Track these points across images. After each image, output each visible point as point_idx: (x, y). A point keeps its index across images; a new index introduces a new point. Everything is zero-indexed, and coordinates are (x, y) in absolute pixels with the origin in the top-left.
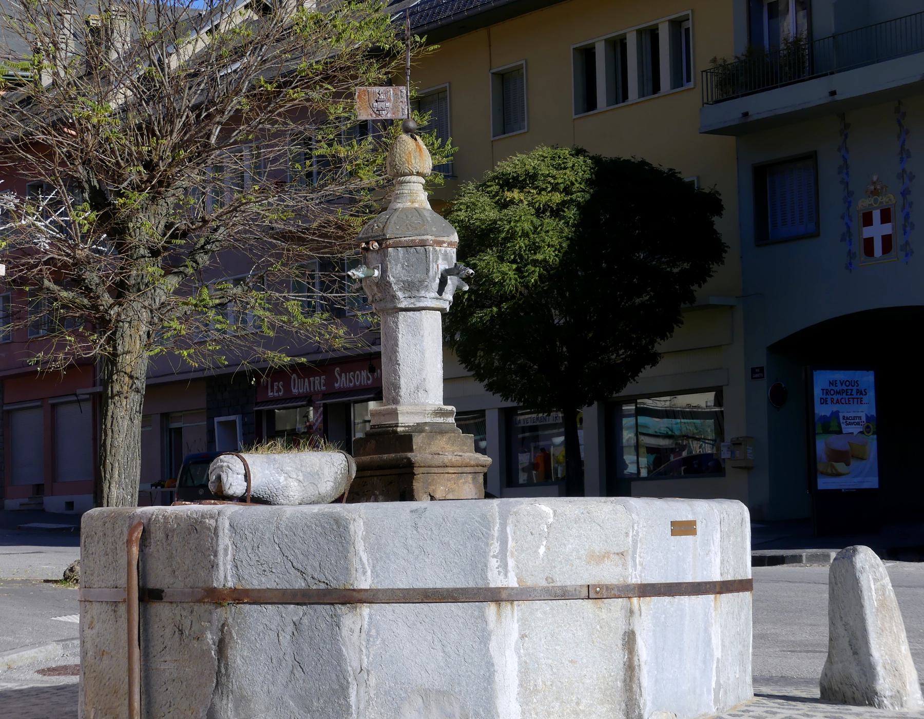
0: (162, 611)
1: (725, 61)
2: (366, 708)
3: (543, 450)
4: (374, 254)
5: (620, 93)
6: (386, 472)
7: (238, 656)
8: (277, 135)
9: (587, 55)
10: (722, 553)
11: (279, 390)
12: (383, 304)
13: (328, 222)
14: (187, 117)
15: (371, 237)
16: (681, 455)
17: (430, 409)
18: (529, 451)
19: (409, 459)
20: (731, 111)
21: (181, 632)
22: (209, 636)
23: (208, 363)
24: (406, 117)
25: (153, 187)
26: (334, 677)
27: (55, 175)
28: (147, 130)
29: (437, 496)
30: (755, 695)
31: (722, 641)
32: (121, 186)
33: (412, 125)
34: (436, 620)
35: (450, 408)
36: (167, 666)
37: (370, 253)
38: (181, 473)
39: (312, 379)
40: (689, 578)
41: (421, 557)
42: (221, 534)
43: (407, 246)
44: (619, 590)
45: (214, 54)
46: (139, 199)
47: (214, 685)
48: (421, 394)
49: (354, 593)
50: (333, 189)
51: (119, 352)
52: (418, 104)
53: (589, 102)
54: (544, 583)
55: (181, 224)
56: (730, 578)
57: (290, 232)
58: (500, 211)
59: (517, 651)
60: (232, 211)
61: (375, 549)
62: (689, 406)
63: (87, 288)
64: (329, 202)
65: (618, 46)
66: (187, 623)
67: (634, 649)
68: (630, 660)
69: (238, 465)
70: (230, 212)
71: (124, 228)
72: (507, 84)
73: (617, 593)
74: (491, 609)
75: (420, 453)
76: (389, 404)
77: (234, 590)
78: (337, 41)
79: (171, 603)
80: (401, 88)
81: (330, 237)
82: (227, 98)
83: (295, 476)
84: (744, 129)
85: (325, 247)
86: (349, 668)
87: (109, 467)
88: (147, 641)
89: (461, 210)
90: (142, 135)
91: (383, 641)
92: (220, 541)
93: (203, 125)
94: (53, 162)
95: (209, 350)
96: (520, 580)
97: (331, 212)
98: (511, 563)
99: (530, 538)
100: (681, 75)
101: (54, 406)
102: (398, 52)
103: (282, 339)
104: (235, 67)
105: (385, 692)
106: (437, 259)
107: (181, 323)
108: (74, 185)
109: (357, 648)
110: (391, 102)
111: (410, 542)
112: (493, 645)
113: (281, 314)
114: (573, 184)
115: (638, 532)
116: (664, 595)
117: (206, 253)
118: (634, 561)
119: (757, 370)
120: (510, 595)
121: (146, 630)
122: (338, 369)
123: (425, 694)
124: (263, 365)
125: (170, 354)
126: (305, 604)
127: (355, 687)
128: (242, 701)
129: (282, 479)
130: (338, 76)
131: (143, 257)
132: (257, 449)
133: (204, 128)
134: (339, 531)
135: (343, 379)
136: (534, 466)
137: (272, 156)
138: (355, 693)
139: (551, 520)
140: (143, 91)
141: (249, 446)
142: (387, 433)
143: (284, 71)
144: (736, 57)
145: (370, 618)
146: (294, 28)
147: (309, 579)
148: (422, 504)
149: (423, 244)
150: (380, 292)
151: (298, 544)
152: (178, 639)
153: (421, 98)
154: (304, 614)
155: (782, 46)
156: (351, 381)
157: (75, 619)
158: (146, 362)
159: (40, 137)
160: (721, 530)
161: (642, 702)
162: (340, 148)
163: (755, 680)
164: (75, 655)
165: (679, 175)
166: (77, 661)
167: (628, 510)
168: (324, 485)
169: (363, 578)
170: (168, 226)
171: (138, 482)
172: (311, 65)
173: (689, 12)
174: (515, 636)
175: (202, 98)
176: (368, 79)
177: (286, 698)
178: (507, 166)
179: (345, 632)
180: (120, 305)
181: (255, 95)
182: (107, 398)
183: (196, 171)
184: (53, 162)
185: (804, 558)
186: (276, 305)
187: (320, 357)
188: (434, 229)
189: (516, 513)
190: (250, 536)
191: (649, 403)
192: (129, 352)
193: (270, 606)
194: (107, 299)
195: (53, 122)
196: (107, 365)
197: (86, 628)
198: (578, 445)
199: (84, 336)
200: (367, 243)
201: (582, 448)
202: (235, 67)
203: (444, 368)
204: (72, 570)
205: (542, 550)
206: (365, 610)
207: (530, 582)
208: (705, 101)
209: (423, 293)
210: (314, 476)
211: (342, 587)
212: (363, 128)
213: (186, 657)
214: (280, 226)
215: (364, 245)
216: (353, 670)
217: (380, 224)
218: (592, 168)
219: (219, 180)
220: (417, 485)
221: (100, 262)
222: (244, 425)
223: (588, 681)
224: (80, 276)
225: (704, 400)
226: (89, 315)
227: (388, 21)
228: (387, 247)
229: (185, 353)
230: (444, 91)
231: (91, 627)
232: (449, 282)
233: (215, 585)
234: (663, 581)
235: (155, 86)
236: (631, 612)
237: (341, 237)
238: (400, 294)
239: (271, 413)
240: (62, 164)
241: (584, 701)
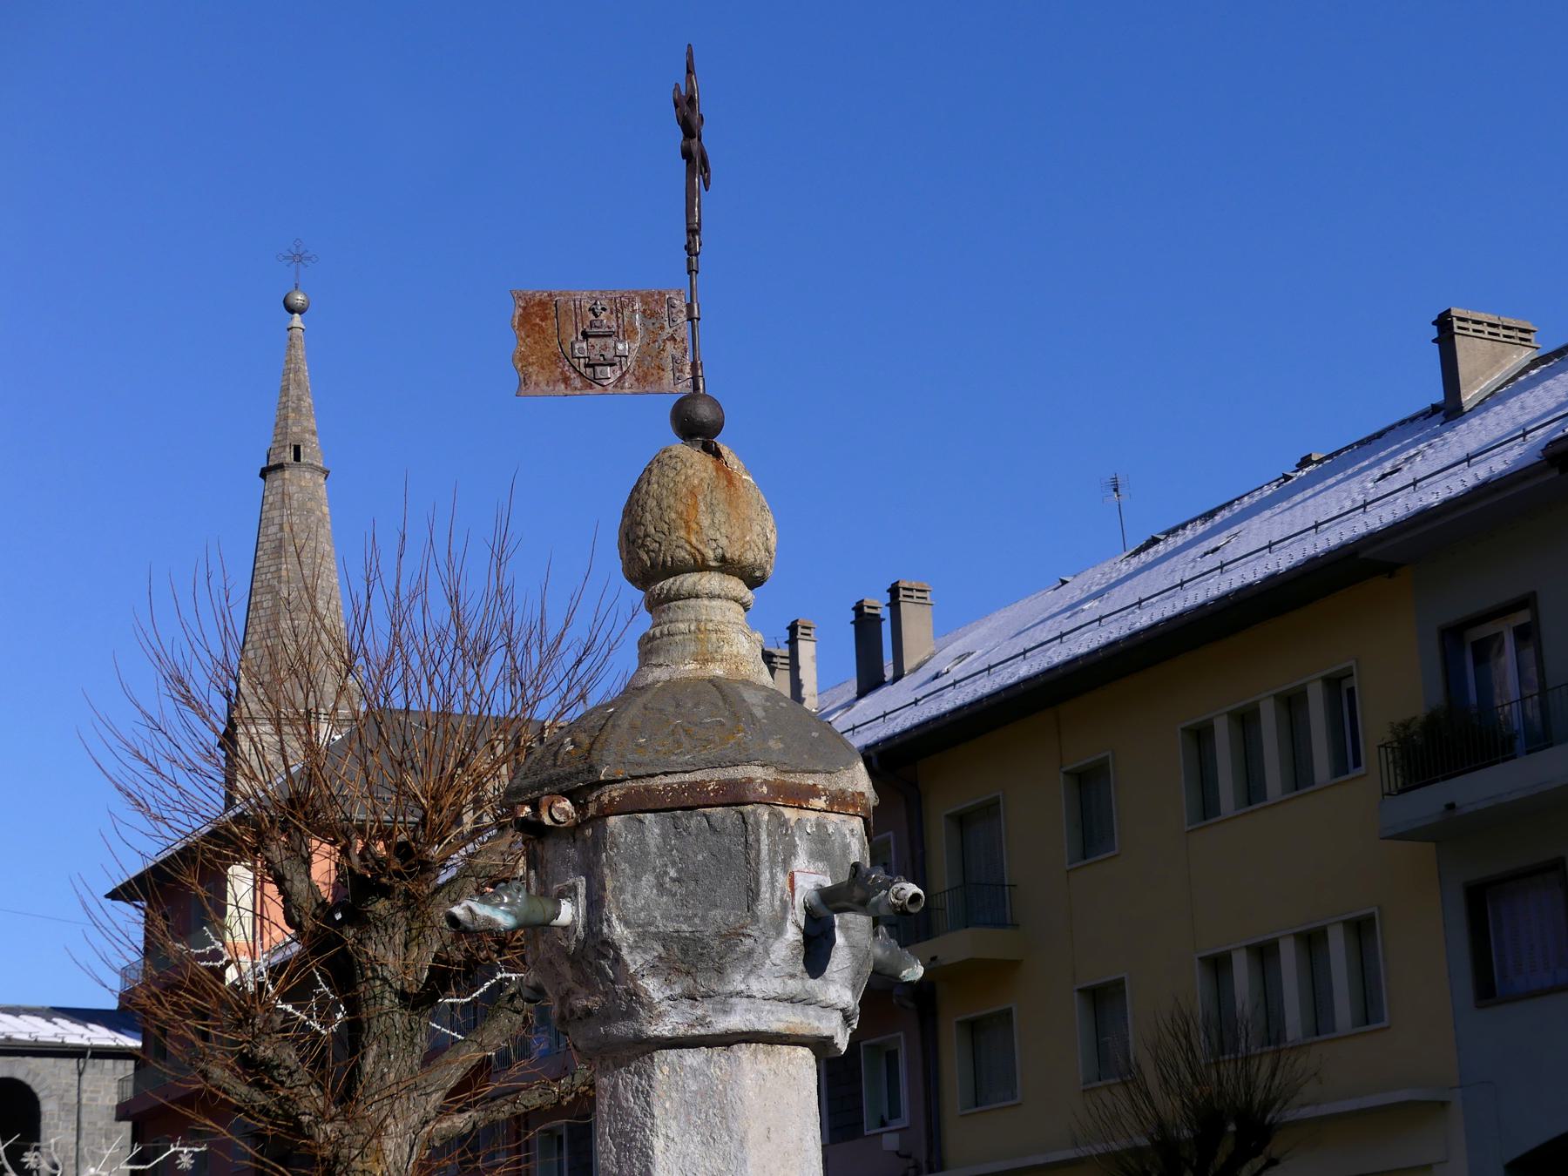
20: (1429, 801)
37: (550, 842)
53: (1208, 807)
72: (1088, 783)
84: (1450, 833)
106: (791, 852)
149: (734, 796)
188: (774, 744)
194: (311, 1100)
200: (535, 806)
209: (737, 982)
228: (604, 813)
238: (652, 987)
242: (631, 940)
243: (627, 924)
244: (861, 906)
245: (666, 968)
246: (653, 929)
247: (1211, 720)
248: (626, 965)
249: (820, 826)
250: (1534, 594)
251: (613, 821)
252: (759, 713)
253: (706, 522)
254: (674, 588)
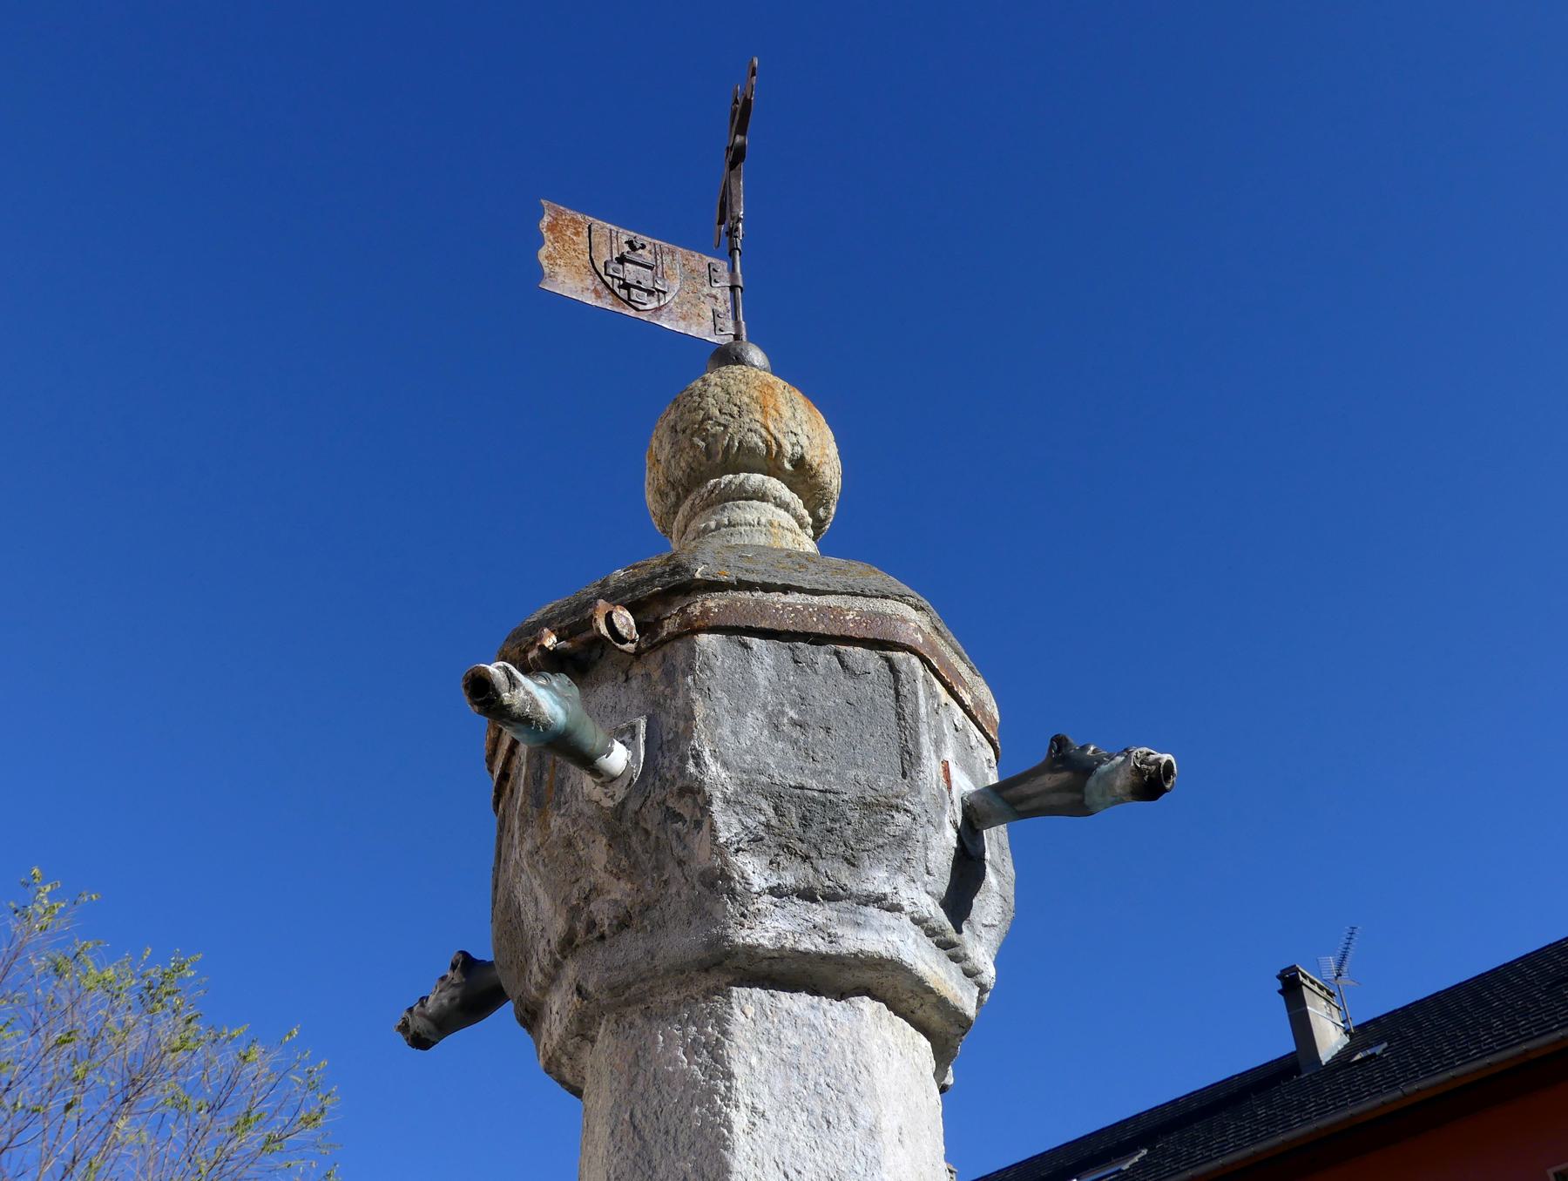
12: (632, 947)
228: (691, 630)
238: (753, 870)
242: (730, 789)
243: (725, 765)
245: (777, 843)
246: (764, 779)
248: (713, 829)
251: (703, 638)
254: (737, 481)
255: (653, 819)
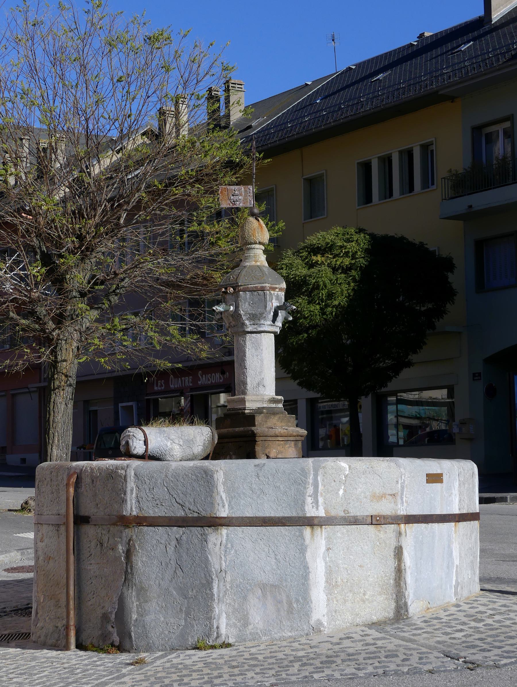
0: (89, 531)
1: (457, 171)
2: (224, 596)
3: (335, 426)
4: (230, 296)
5: (409, 186)
6: (237, 439)
7: (140, 561)
8: (165, 217)
9: (366, 168)
10: (460, 495)
11: (161, 386)
13: (197, 275)
14: (105, 206)
15: (229, 284)
16: (425, 430)
17: (266, 398)
18: (326, 427)
19: (253, 431)
20: (461, 205)
21: (102, 544)
22: (120, 547)
23: (117, 367)
24: (252, 206)
25: (82, 252)
26: (203, 576)
27: (18, 243)
28: (78, 214)
29: (271, 455)
30: (481, 590)
31: (460, 554)
32: (62, 251)
33: (256, 211)
34: (271, 538)
35: (279, 397)
36: (92, 567)
37: (228, 295)
38: (101, 438)
39: (183, 378)
40: (438, 511)
41: (261, 496)
42: (128, 480)
43: (252, 291)
44: (392, 519)
45: (124, 165)
46: (72, 260)
47: (123, 580)
48: (261, 388)
49: (217, 519)
50: (201, 253)
51: (58, 360)
52: (258, 198)
54: (342, 514)
55: (100, 276)
56: (465, 511)
57: (172, 281)
58: (309, 269)
59: (324, 559)
60: (134, 268)
61: (231, 490)
62: (431, 398)
63: (38, 318)
64: (198, 262)
65: (386, 162)
66: (105, 539)
67: (401, 558)
68: (399, 565)
69: (140, 435)
70: (132, 268)
71: (63, 278)
72: (314, 187)
73: (391, 521)
74: (307, 531)
75: (261, 427)
76: (240, 395)
77: (137, 517)
78: (205, 156)
79: (95, 525)
80: (249, 187)
81: (198, 285)
82: (132, 194)
83: (176, 443)
84: (469, 217)
85: (195, 291)
86: (213, 570)
87: (51, 436)
88: (79, 550)
89: (282, 269)
90: (75, 218)
91: (236, 551)
92: (128, 485)
93: (115, 211)
94: (18, 235)
95: (118, 359)
96: (326, 512)
97: (199, 268)
98: (321, 500)
99: (333, 484)
100: (428, 180)
101: (13, 395)
102: (244, 164)
103: (166, 351)
104: (136, 173)
105: (237, 585)
106: (272, 299)
107: (100, 341)
108: (30, 250)
109: (219, 557)
110: (243, 196)
111: (254, 486)
112: (308, 555)
113: (166, 335)
114: (357, 252)
115: (404, 481)
116: (422, 522)
117: (116, 295)
118: (402, 499)
119: (477, 375)
120: (320, 522)
121: (78, 543)
122: (200, 372)
123: (263, 587)
124: (153, 369)
125: (93, 361)
126: (184, 527)
127: (217, 582)
128: (142, 591)
129: (169, 444)
130: (207, 179)
131: (75, 297)
132: (152, 424)
133: (116, 213)
134: (207, 478)
135: (204, 378)
136: (329, 437)
137: (161, 231)
138: (217, 586)
139: (347, 472)
140: (76, 189)
141: (147, 423)
142: (238, 414)
143: (169, 175)
144: (465, 169)
145: (227, 536)
146: (177, 147)
147: (187, 510)
148: (261, 461)
149: (263, 289)
150: (235, 321)
151: (180, 487)
152: (99, 549)
153: (260, 194)
154: (184, 533)
155: (495, 162)
156: (209, 380)
157: (31, 535)
158: (76, 366)
159: (9, 219)
160: (459, 480)
161: (407, 594)
162: (206, 226)
163: (481, 580)
164: (29, 559)
165: (426, 246)
166: (32, 563)
167: (398, 466)
168: (197, 448)
169: (223, 510)
170: (93, 276)
171: (70, 446)
172: (188, 172)
173: (433, 139)
174: (323, 549)
175: (115, 193)
176: (224, 182)
177: (171, 589)
178: (316, 239)
179: (210, 545)
180: (60, 329)
181: (150, 192)
182: (51, 390)
183: (111, 241)
184: (18, 235)
185: (509, 499)
186: (162, 329)
187: (191, 364)
188: (270, 280)
189: (324, 467)
190: (148, 481)
191: (405, 396)
192: (65, 361)
193: (160, 528)
194: (51, 325)
195: (18, 208)
196: (51, 368)
197: (38, 541)
198: (359, 423)
199: (35, 349)
200: (226, 289)
201: (361, 424)
202: (136, 173)
203: (276, 371)
204: (26, 503)
205: (341, 492)
206: (224, 531)
207: (333, 513)
208: (444, 198)
209: (262, 322)
210: (190, 442)
211: (209, 516)
212: (219, 215)
213: (105, 561)
214: (165, 277)
215: (223, 290)
216: (216, 571)
217: (234, 276)
218: (369, 241)
219: (125, 247)
220: (258, 449)
221: (47, 301)
222: (138, 408)
223: (371, 579)
224: (33, 310)
225: (441, 394)
226: (39, 336)
227: (239, 143)
228: (239, 291)
229: (103, 360)
230: (272, 190)
231: (42, 541)
232: (280, 314)
233: (124, 513)
234: (421, 513)
235: (84, 185)
236: (400, 534)
237: (206, 285)
238: (247, 322)
239: (156, 401)
240: (23, 236)
241: (368, 593)
244: (285, 309)
245: (249, 319)
247: (371, 160)
249: (277, 294)
250: (513, 115)
251: (241, 292)
252: (267, 273)
253: (257, 235)
255: (236, 316)
